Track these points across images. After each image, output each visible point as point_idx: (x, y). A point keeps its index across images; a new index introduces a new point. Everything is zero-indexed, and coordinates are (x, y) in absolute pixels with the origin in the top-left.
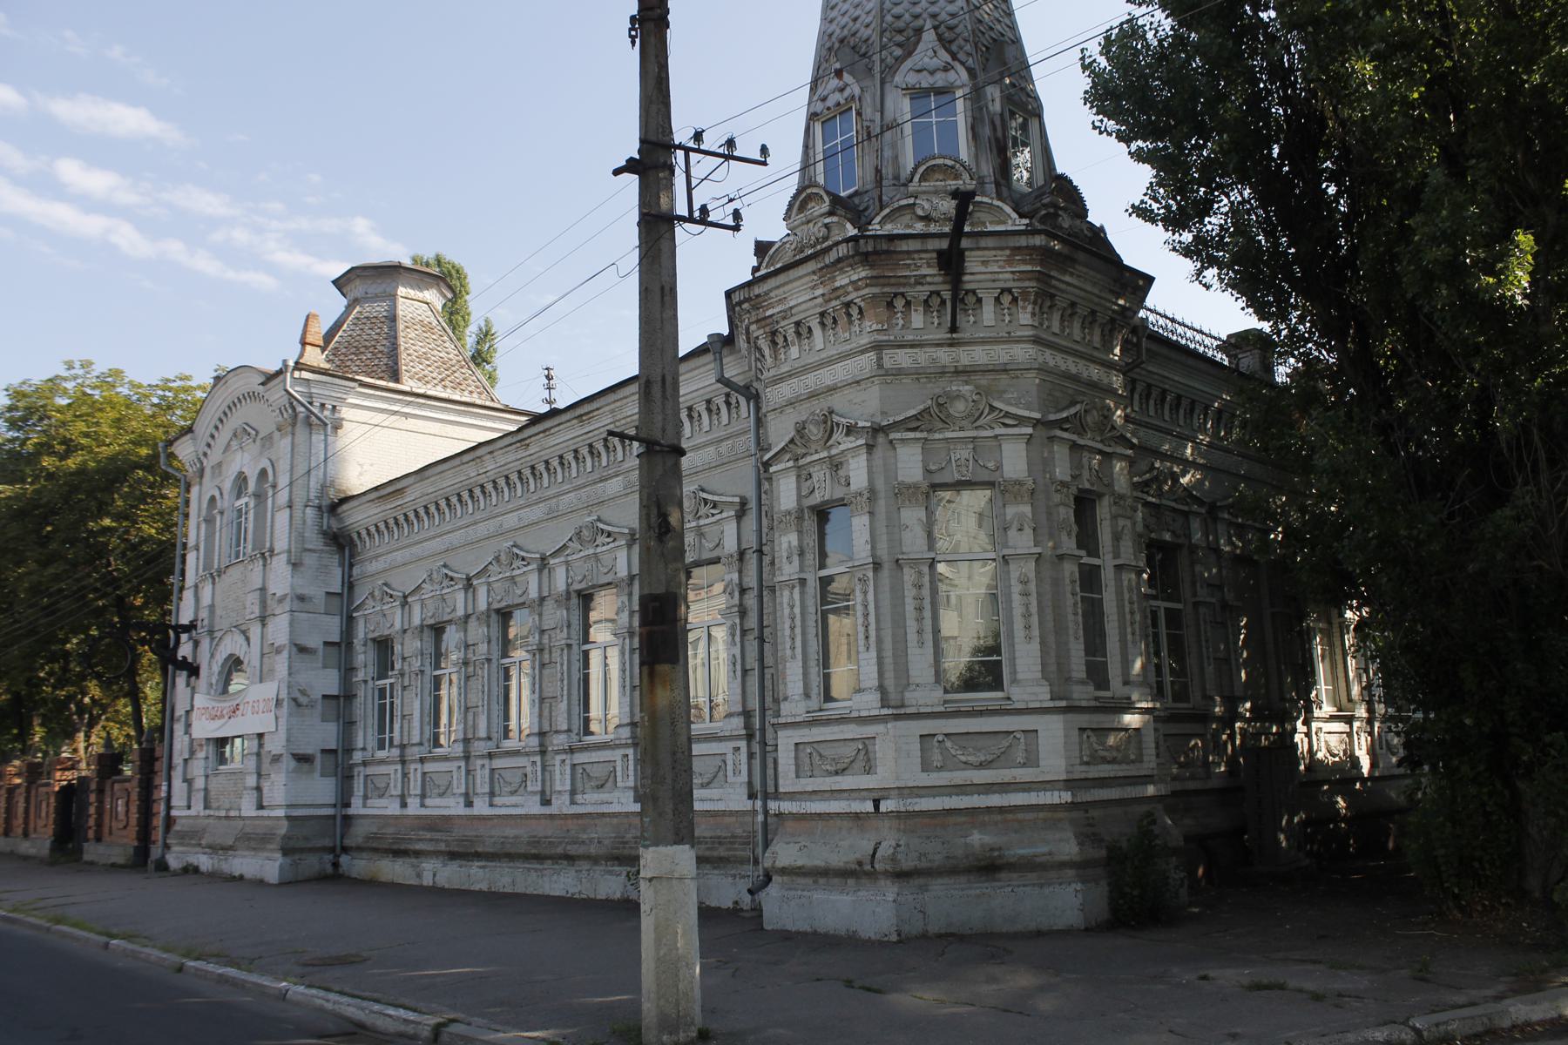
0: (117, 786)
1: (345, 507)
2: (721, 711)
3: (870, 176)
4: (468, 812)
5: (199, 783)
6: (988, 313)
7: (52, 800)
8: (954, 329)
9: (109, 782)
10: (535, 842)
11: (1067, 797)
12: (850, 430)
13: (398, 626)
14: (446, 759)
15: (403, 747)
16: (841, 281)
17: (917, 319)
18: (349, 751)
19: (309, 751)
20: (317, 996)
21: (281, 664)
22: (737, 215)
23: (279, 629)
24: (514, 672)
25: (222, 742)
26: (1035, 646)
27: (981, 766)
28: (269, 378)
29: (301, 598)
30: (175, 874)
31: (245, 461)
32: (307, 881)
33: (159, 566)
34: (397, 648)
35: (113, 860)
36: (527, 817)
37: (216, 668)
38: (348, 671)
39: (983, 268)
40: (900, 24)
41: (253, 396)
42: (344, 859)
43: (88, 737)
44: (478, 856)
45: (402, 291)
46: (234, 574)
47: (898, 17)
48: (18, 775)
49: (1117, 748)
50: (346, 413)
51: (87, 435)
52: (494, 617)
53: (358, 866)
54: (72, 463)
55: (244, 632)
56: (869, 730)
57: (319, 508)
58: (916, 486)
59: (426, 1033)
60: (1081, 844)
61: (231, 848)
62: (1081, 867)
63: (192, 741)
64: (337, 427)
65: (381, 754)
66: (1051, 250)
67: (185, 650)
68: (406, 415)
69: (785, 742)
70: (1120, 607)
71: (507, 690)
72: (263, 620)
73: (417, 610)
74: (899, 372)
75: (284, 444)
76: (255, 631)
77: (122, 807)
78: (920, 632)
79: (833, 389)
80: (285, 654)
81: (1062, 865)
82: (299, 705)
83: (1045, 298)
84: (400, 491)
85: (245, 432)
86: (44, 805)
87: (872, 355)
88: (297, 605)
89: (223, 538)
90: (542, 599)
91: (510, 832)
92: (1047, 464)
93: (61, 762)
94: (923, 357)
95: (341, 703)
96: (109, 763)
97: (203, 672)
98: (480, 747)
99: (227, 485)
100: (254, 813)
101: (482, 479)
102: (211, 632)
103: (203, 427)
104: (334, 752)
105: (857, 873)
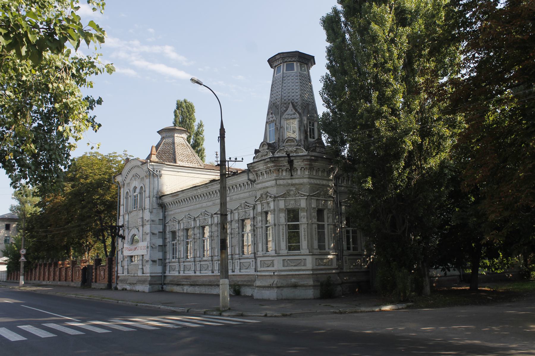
0: (101, 268)
1: (163, 197)
2: (250, 253)
3: (277, 139)
4: (195, 274)
5: (126, 267)
6: (299, 172)
7: (81, 271)
8: (292, 176)
9: (98, 267)
10: (210, 282)
11: (311, 272)
12: (270, 197)
13: (177, 228)
14: (189, 262)
15: (179, 259)
16: (269, 165)
17: (284, 174)
18: (165, 259)
19: (155, 259)
20: (166, 308)
21: (148, 238)
22: (242, 159)
23: (147, 228)
24: (205, 241)
25: (132, 257)
26: (306, 242)
27: (295, 266)
28: (143, 163)
29: (153, 221)
30: (120, 290)
31: (136, 183)
32: (155, 292)
33: (112, 207)
34: (177, 234)
35: (101, 287)
36: (208, 276)
37: (130, 237)
38: (165, 239)
39: (298, 164)
40: (285, 102)
41: (138, 166)
42: (164, 286)
43: (88, 253)
44: (197, 285)
45: (176, 135)
46: (134, 213)
47: (285, 100)
48: (68, 264)
49: (326, 263)
50: (163, 172)
51: (91, 173)
52: (201, 228)
53: (167, 288)
54: (88, 181)
55: (137, 229)
56: (273, 258)
57: (157, 197)
58: (283, 209)
59: (186, 311)
60: (314, 282)
61: (136, 284)
62: (314, 286)
63: (123, 256)
64: (161, 176)
65: (173, 260)
66: (312, 159)
67: (121, 232)
68: (178, 172)
69: (259, 260)
70: (328, 233)
71: (204, 245)
72: (143, 226)
73: (182, 225)
74: (280, 185)
75: (148, 180)
76: (141, 229)
77: (103, 273)
78: (283, 239)
79: (267, 187)
80: (149, 235)
81: (310, 286)
82: (153, 248)
83: (311, 168)
84: (178, 195)
85: (136, 176)
86: (78, 273)
87: (275, 181)
88: (152, 223)
89: (131, 201)
90: (212, 224)
91: (205, 279)
92: (310, 204)
93: (83, 260)
94: (285, 182)
95: (163, 247)
96: (98, 261)
97: (126, 238)
98: (197, 259)
99: (132, 189)
100: (141, 275)
101: (198, 194)
102: (128, 228)
103: (124, 172)
104: (161, 259)
105: (270, 287)
